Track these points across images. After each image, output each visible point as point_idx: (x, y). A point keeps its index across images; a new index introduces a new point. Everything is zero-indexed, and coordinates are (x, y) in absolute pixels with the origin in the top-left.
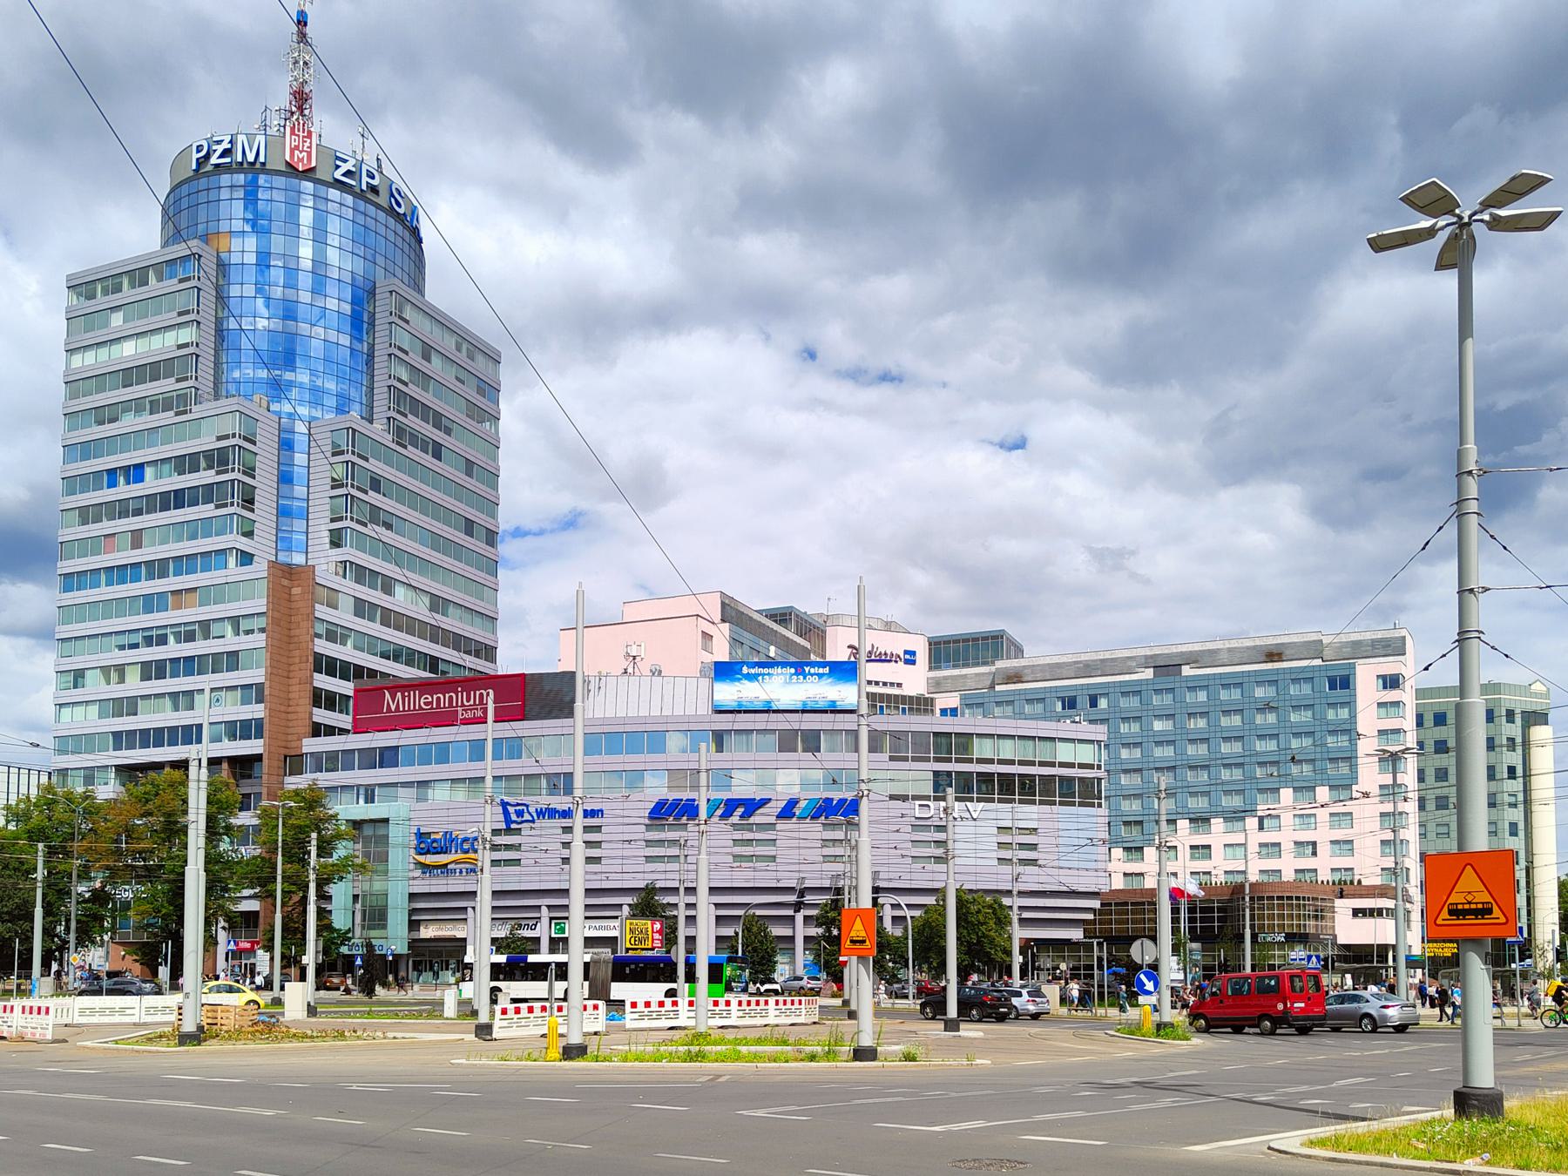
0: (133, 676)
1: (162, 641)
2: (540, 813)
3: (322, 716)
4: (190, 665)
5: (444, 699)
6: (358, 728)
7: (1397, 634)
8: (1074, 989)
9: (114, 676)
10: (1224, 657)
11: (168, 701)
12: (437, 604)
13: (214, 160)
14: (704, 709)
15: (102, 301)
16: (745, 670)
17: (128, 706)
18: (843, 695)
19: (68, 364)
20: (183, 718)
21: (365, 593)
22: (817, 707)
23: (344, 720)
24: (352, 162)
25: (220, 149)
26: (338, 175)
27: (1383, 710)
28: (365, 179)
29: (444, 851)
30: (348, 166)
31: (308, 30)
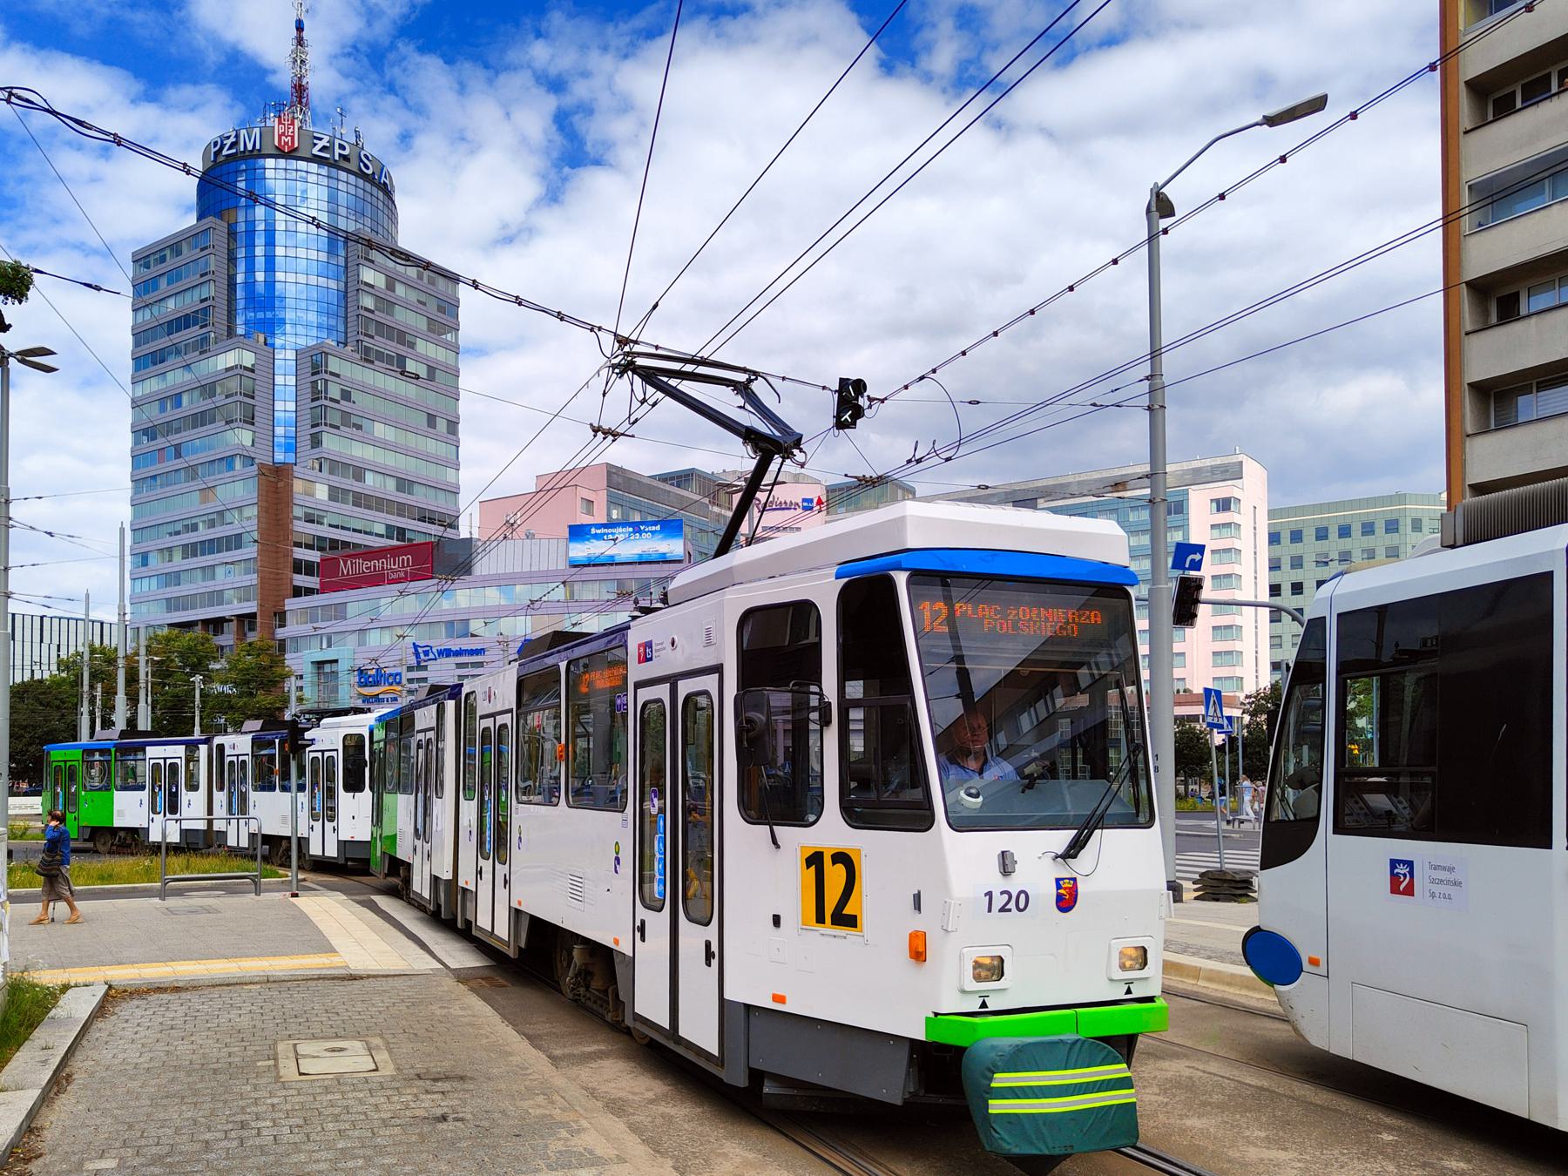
0: (177, 556)
1: (195, 528)
2: (441, 653)
3: (301, 580)
4: (211, 546)
5: (378, 564)
6: (324, 589)
7: (1234, 459)
8: (239, 744)
9: (167, 554)
10: (1075, 490)
11: (199, 573)
12: (404, 484)
13: (225, 152)
14: (562, 565)
15: (156, 270)
16: (593, 531)
17: (174, 578)
18: (672, 548)
19: (135, 319)
20: (211, 586)
21: (337, 481)
22: (652, 558)
23: (312, 582)
24: (327, 138)
25: (228, 142)
26: (315, 151)
27: (1216, 532)
28: (337, 151)
29: (377, 684)
30: (324, 143)
31: (305, 34)
